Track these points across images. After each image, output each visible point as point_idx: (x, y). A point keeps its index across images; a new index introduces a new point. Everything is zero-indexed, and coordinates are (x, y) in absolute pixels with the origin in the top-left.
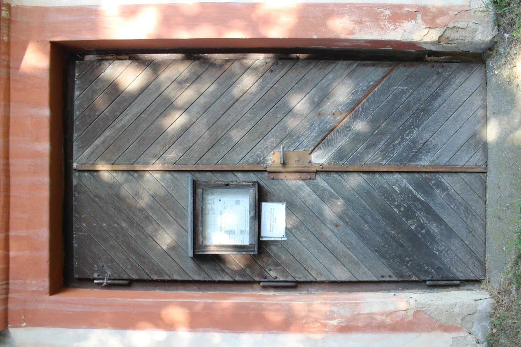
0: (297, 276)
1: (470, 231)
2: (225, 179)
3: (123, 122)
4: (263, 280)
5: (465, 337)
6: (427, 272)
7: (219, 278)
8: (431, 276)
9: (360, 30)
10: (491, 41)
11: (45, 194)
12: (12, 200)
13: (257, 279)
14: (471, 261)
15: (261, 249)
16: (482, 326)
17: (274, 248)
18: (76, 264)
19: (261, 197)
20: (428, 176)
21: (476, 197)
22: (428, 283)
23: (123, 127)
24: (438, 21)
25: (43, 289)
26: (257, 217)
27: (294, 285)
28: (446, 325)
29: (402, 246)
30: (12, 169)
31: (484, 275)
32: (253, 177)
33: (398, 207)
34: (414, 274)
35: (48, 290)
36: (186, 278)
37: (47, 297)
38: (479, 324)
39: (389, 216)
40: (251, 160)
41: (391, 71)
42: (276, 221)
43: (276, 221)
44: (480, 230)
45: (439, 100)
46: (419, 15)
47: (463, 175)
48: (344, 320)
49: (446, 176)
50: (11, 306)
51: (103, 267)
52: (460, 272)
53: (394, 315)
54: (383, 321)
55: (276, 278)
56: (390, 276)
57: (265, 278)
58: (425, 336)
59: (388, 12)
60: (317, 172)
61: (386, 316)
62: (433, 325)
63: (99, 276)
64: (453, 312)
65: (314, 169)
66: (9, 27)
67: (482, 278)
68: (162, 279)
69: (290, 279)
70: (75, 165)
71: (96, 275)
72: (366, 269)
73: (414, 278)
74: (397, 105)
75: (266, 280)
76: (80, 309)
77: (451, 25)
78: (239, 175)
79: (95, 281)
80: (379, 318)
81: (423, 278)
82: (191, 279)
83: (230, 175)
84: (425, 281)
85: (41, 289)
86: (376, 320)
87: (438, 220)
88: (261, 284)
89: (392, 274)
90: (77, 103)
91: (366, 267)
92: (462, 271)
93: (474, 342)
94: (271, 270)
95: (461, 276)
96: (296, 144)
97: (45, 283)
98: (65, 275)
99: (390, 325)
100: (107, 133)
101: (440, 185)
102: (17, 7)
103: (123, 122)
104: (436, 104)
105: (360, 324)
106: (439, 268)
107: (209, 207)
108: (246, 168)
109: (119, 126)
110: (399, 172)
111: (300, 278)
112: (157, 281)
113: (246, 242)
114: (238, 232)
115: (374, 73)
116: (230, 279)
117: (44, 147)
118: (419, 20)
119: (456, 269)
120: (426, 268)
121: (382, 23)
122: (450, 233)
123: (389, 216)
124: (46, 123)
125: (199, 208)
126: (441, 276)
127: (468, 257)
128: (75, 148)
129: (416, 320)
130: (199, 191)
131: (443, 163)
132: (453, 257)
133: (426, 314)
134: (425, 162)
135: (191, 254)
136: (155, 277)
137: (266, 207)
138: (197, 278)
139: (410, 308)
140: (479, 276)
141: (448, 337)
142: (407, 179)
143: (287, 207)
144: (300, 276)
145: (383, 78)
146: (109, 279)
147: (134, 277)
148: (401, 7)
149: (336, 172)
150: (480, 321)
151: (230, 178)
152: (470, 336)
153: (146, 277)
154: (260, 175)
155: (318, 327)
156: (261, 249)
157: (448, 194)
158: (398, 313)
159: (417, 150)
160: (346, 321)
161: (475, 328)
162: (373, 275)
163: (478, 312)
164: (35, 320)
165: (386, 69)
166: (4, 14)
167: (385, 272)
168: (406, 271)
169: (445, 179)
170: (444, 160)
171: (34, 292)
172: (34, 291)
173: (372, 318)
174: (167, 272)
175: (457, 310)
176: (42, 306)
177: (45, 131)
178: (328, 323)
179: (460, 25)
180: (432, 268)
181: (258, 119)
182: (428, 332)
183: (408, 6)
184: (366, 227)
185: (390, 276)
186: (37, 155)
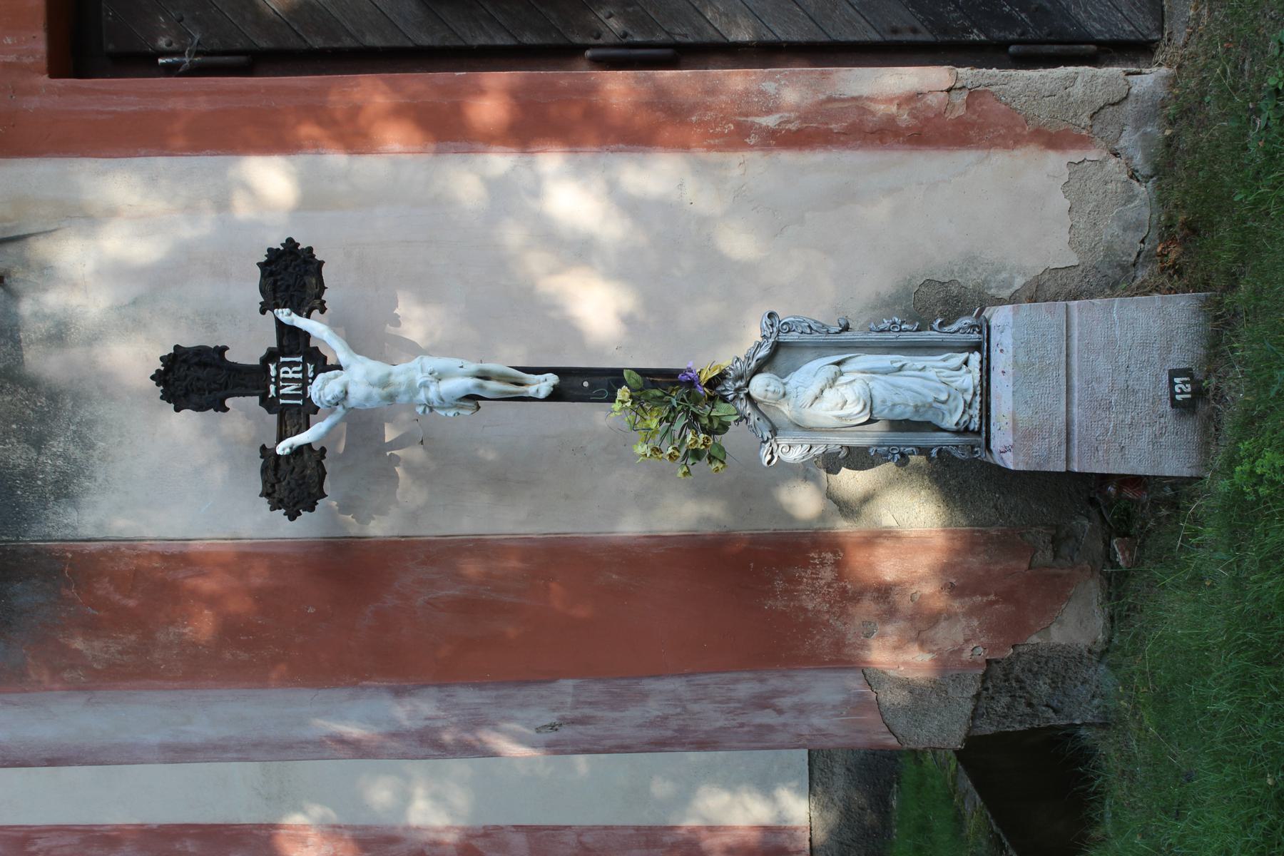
0: (678, 30)
4: (592, 41)
5: (1102, 163)
6: (1009, 22)
7: (482, 40)
8: (1019, 31)
13: (578, 40)
16: (1145, 134)
22: (1012, 49)
25: (31, 60)
28: (1053, 130)
31: (1161, 30)
34: (974, 25)
35: (44, 64)
37: (44, 79)
38: (1137, 129)
48: (792, 115)
51: (181, 20)
52: (1095, 20)
53: (919, 105)
54: (891, 119)
55: (625, 35)
56: (914, 31)
57: (598, 37)
58: (999, 158)
61: (899, 105)
62: (1018, 130)
63: (170, 44)
64: (1069, 96)
67: (1155, 37)
68: (335, 45)
69: (660, 37)
71: (162, 43)
72: (851, 10)
73: (976, 36)
75: (601, 41)
79: (161, 61)
80: (881, 109)
81: (997, 34)
82: (410, 44)
85: (27, 60)
86: (873, 113)
88: (588, 53)
89: (918, 25)
91: (852, 6)
92: (1101, 18)
93: (1125, 177)
94: (611, 16)
95: (1096, 29)
97: (37, 45)
99: (908, 128)
106: (1040, 8)
111: (686, 36)
116: (509, 41)
119: (1086, 11)
120: (1007, 9)
126: (1046, 30)
129: (974, 117)
133: (999, 100)
136: (318, 43)
138: (425, 40)
139: (958, 85)
140: (1146, 32)
141: (1056, 161)
144: (684, 30)
146: (198, 53)
147: (264, 44)
150: (1141, 119)
152: (1114, 160)
153: (293, 43)
155: (730, 132)
158: (930, 97)
160: (799, 117)
161: (1128, 140)
162: (869, 27)
163: (1131, 98)
172: (10, 63)
173: (864, 111)
174: (349, 27)
176: (32, 103)
178: (753, 123)
180: (1022, 11)
182: (1006, 147)
185: (914, 31)
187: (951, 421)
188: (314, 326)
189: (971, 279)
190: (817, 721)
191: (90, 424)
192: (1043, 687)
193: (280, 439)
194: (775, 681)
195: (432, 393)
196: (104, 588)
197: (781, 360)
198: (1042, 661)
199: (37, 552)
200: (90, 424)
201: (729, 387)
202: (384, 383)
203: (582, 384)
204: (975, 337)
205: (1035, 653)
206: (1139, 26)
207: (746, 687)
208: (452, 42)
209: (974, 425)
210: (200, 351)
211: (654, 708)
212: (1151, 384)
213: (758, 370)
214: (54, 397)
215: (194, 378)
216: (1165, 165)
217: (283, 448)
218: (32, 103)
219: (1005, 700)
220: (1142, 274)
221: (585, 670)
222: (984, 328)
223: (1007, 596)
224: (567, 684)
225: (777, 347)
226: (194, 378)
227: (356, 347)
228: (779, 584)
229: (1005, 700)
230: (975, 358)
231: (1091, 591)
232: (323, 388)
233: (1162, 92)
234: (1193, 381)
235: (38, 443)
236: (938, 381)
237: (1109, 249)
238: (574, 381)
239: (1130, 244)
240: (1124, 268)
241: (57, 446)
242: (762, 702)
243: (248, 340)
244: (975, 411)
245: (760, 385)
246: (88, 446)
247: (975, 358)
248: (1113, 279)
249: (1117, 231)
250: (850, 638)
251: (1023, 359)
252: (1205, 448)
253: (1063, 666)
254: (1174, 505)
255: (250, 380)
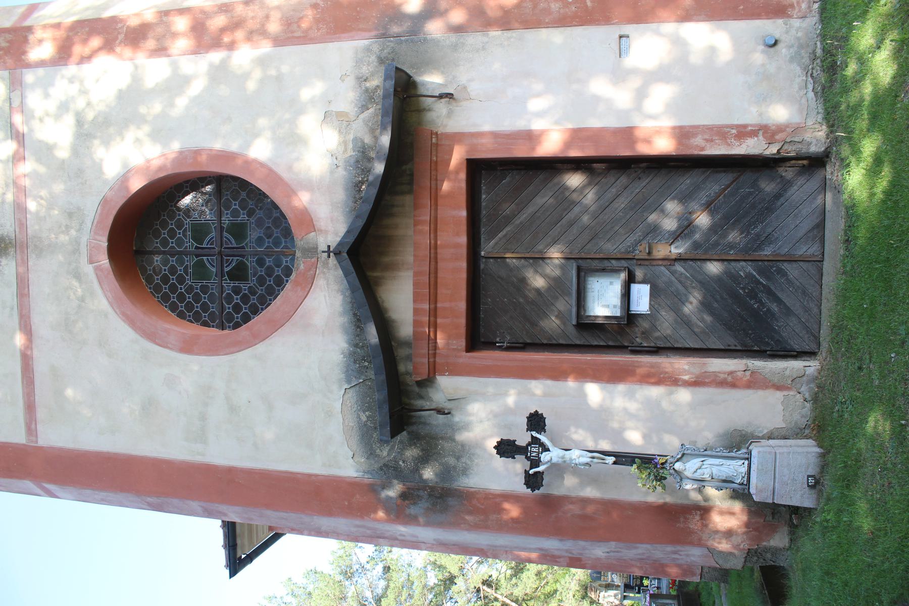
1: (807, 310)
2: (604, 268)
3: (522, 219)
6: (768, 344)
7: (596, 343)
9: (711, 147)
10: (824, 152)
11: (464, 275)
12: (439, 280)
13: (626, 344)
14: (806, 336)
15: (629, 318)
17: (640, 319)
18: (482, 330)
19: (631, 280)
20: (770, 263)
21: (812, 282)
23: (521, 223)
24: (777, 137)
26: (626, 295)
27: (656, 351)
29: (746, 321)
30: (439, 256)
32: (624, 264)
33: (743, 289)
36: (570, 342)
39: (735, 296)
40: (623, 250)
41: (739, 176)
42: (642, 299)
43: (642, 299)
44: (816, 310)
45: (782, 200)
46: (761, 133)
47: (801, 264)
49: (785, 264)
50: (438, 360)
54: (725, 379)
58: (761, 393)
59: (734, 131)
60: (676, 260)
65: (673, 257)
66: (437, 150)
69: (652, 345)
70: (483, 253)
71: (498, 340)
73: (756, 348)
74: (744, 205)
76: (489, 363)
77: (788, 140)
78: (613, 262)
80: (722, 376)
81: (763, 348)
83: (606, 261)
84: (766, 351)
87: (779, 301)
90: (484, 204)
95: (797, 347)
96: (659, 237)
97: (463, 343)
98: (477, 338)
100: (508, 229)
101: (780, 271)
102: (442, 134)
103: (522, 219)
104: (779, 203)
105: (707, 380)
107: (589, 286)
108: (619, 256)
109: (518, 222)
110: (745, 260)
112: (546, 345)
113: (618, 314)
114: (611, 306)
115: (725, 178)
117: (463, 239)
118: (761, 137)
121: (729, 141)
122: (788, 312)
123: (735, 296)
124: (464, 222)
125: (582, 287)
127: (804, 332)
128: (482, 240)
130: (582, 274)
131: (783, 253)
132: (791, 331)
134: (767, 252)
135: (574, 322)
137: (635, 288)
138: (578, 342)
141: (779, 395)
142: (751, 266)
143: (103, 173)
145: (732, 183)
147: (528, 341)
148: (745, 126)
149: (692, 260)
150: (808, 382)
151: (606, 264)
153: (537, 341)
154: (630, 262)
156: (629, 318)
157: (787, 279)
159: (760, 242)
164: (456, 371)
165: (735, 175)
166: (434, 140)
167: (731, 342)
168: (749, 342)
169: (785, 266)
170: (785, 250)
171: (454, 349)
173: (717, 376)
175: (787, 373)
177: (464, 228)
179: (796, 139)
181: (628, 217)
183: (751, 125)
184: (716, 305)
186: (457, 246)
187: (738, 482)
188: (542, 438)
189: (749, 430)
190: (692, 558)
191: (473, 454)
192: (769, 556)
193: (531, 468)
194: (678, 548)
195: (577, 462)
196: (475, 502)
197: (684, 458)
198: (767, 550)
199: (456, 490)
200: (473, 454)
201: (667, 466)
202: (563, 457)
203: (623, 459)
204: (747, 456)
205: (765, 547)
206: (813, 347)
207: (669, 548)
208: (587, 343)
209: (745, 483)
210: (509, 441)
211: (640, 551)
212: (802, 478)
213: (677, 461)
214: (463, 446)
215: (506, 448)
216: (815, 399)
217: (531, 472)
218: (461, 360)
219: (756, 558)
220: (807, 431)
221: (618, 540)
222: (750, 453)
223: (756, 529)
224: (613, 543)
225: (683, 455)
226: (506, 448)
227: (555, 445)
228: (682, 519)
229: (756, 558)
230: (746, 462)
231: (786, 529)
232: (545, 457)
233: (816, 374)
234: (815, 479)
235: (458, 458)
236: (734, 468)
237: (796, 423)
238: (620, 459)
239: (803, 422)
240: (801, 430)
241: (463, 460)
242: (675, 553)
243: (523, 438)
244: (745, 479)
245: (678, 466)
246: (472, 461)
247: (746, 462)
248: (797, 433)
249: (799, 417)
250: (704, 538)
251: (760, 467)
252: (818, 499)
253: (776, 551)
254: (810, 512)
255: (523, 450)
